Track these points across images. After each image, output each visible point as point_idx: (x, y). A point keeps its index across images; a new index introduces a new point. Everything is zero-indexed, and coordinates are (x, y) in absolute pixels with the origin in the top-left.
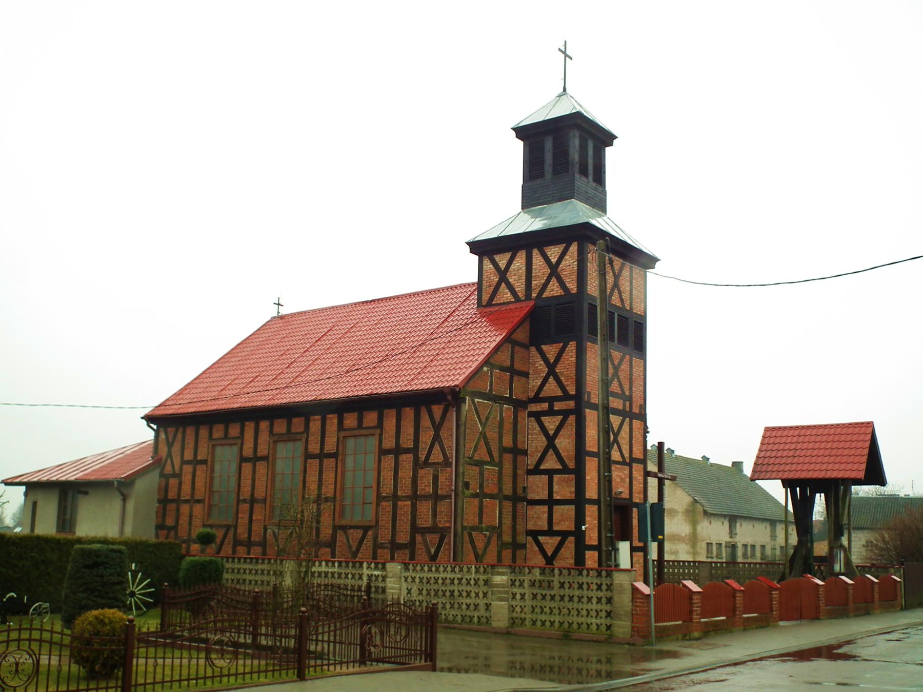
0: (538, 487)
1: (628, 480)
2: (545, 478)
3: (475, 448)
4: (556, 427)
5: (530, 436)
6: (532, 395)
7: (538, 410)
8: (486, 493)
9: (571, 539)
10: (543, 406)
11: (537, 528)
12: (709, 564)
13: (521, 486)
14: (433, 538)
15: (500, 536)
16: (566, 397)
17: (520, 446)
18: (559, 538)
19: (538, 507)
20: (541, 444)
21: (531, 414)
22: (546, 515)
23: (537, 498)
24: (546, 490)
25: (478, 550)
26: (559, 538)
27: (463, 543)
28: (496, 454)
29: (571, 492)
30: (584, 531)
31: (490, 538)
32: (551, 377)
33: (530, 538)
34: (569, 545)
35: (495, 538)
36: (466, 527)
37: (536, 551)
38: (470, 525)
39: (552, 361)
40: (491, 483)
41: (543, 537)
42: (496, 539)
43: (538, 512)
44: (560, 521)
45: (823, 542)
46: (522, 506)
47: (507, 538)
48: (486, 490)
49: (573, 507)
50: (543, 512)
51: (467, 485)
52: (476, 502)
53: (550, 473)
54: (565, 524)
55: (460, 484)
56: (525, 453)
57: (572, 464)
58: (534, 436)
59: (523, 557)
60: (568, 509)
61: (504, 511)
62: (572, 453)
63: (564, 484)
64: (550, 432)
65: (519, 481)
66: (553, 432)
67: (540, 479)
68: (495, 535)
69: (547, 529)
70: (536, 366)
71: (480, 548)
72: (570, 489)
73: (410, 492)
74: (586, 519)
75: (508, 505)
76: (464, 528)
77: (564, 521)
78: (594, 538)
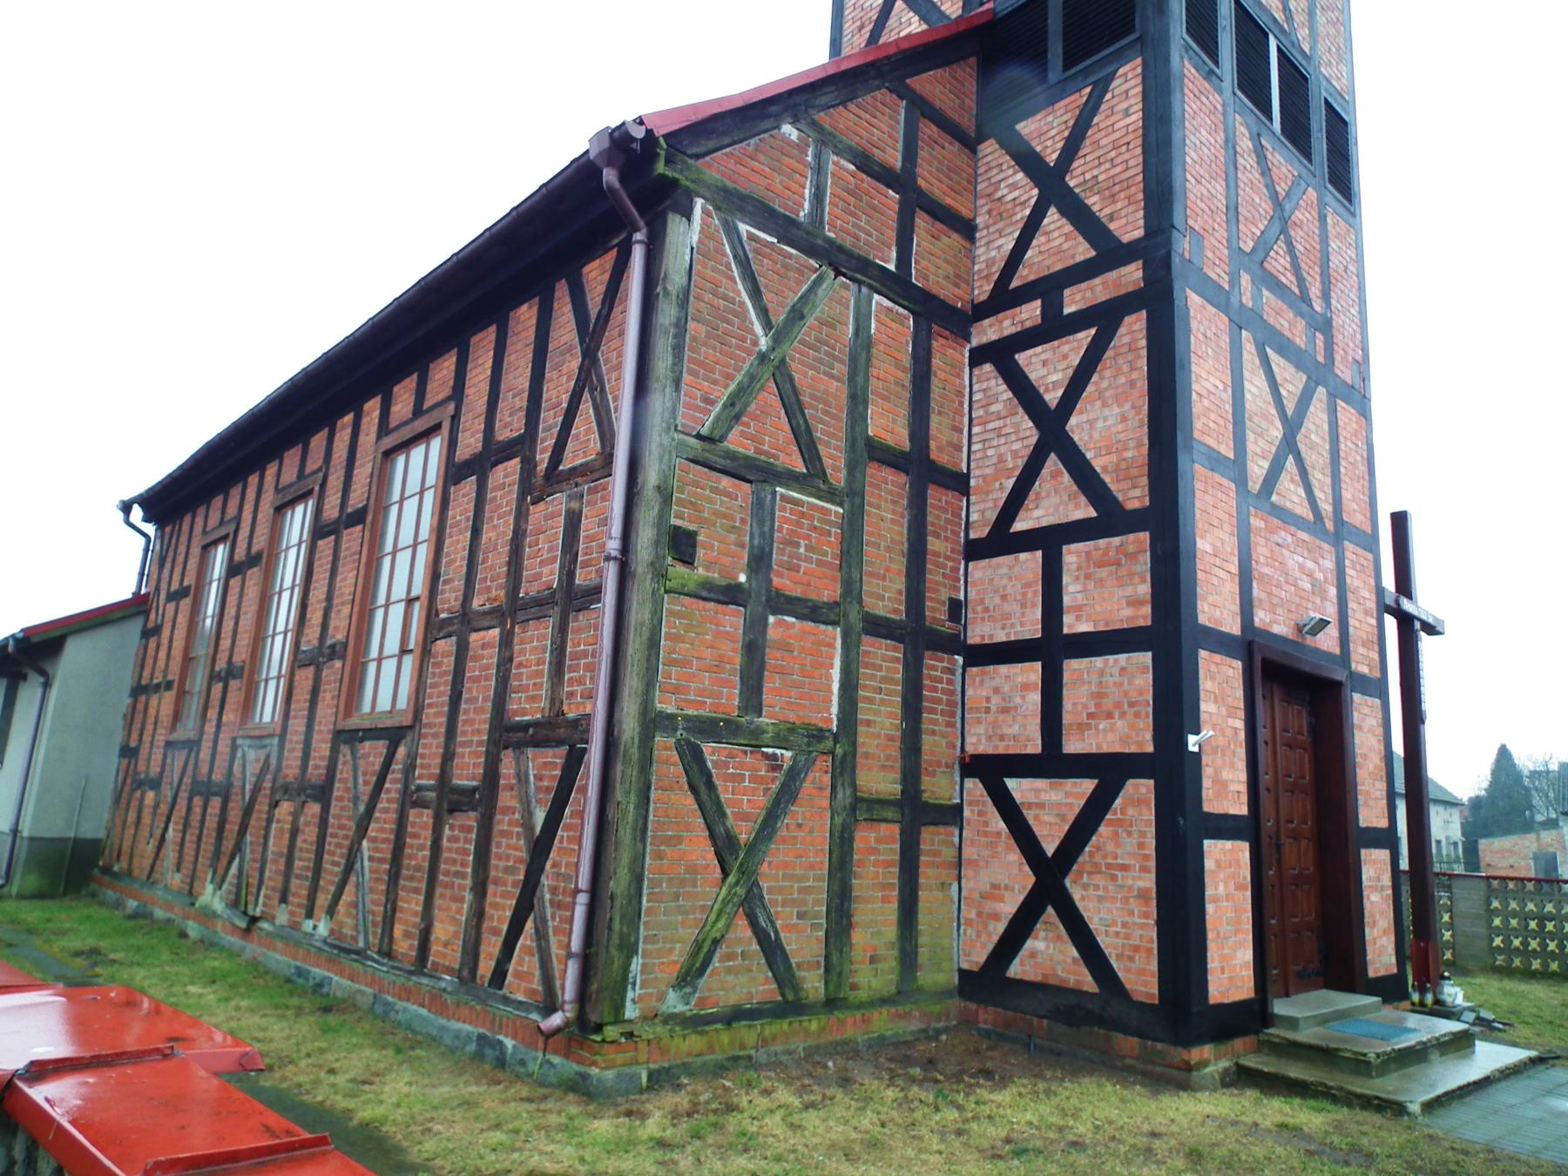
0: (1004, 598)
1: (1333, 591)
2: (1031, 562)
3: (731, 403)
4: (1070, 372)
5: (975, 430)
6: (982, 291)
7: (1007, 332)
8: (778, 593)
9: (1139, 793)
10: (1024, 316)
11: (1001, 748)
12: (1483, 884)
13: (944, 595)
14: (544, 764)
15: (845, 768)
16: (1110, 253)
17: (939, 453)
18: (1087, 786)
19: (1004, 669)
20: (1017, 446)
21: (979, 356)
22: (1035, 698)
23: (1001, 637)
24: (1034, 605)
25: (730, 821)
26: (1087, 786)
27: (646, 788)
28: (834, 459)
29: (1134, 603)
30: (1197, 756)
31: (794, 776)
32: (1053, 210)
33: (974, 786)
34: (1131, 812)
35: (819, 776)
36: (672, 717)
37: (998, 834)
38: (690, 712)
39: (1055, 156)
40: (808, 560)
41: (1027, 783)
42: (827, 779)
43: (1006, 689)
44: (1091, 716)
45: (1528, 836)
46: (936, 666)
47: (879, 779)
48: (782, 582)
49: (1146, 658)
50: (1026, 687)
51: (682, 545)
52: (733, 620)
53: (1051, 541)
54: (1112, 730)
55: (645, 535)
56: (959, 483)
57: (1137, 493)
58: (991, 426)
59: (949, 854)
60: (1123, 670)
61: (868, 679)
62: (1136, 449)
63: (1103, 573)
64: (1047, 397)
65: (934, 575)
66: (1060, 393)
67: (1011, 568)
68: (824, 763)
69: (1039, 750)
70: (999, 194)
71: (744, 817)
72: (1129, 591)
73: (502, 593)
74: (1203, 706)
75: (884, 658)
76: (653, 723)
77: (1110, 716)
78: (1233, 787)
